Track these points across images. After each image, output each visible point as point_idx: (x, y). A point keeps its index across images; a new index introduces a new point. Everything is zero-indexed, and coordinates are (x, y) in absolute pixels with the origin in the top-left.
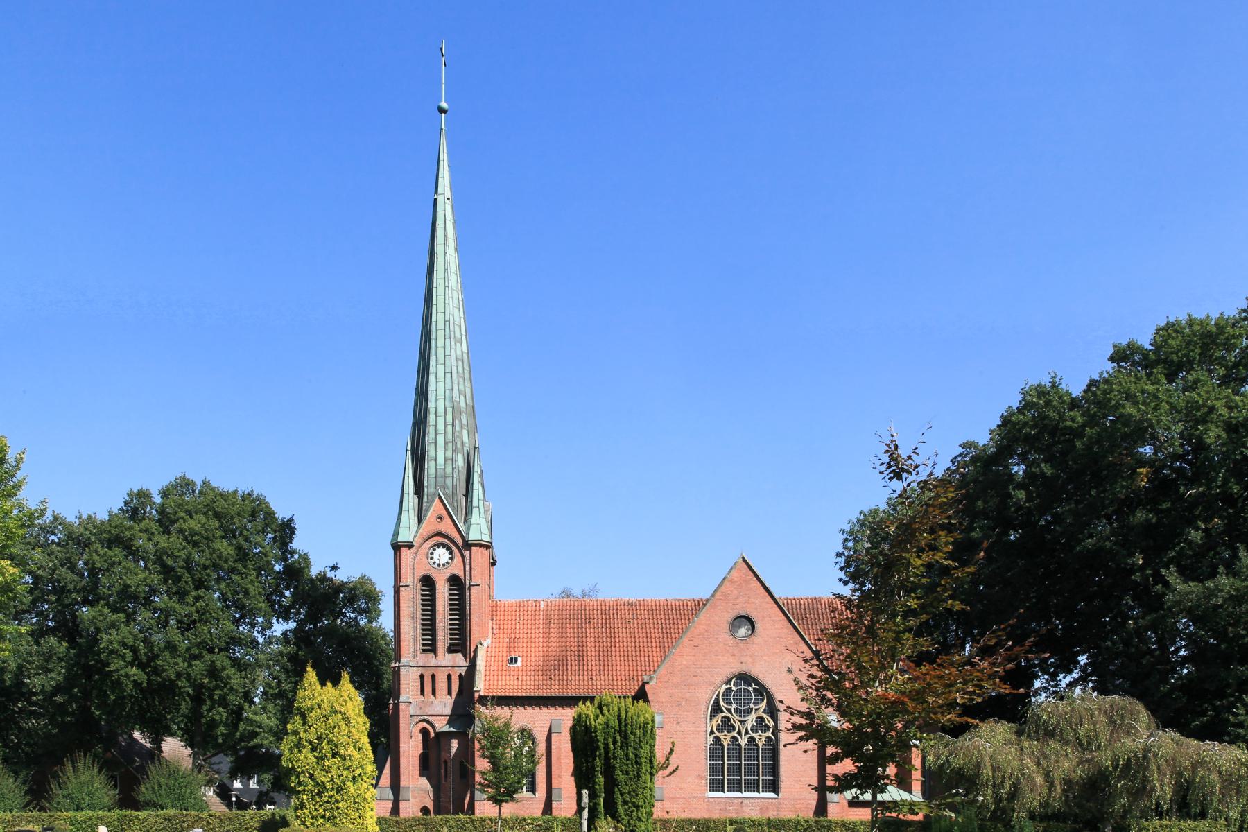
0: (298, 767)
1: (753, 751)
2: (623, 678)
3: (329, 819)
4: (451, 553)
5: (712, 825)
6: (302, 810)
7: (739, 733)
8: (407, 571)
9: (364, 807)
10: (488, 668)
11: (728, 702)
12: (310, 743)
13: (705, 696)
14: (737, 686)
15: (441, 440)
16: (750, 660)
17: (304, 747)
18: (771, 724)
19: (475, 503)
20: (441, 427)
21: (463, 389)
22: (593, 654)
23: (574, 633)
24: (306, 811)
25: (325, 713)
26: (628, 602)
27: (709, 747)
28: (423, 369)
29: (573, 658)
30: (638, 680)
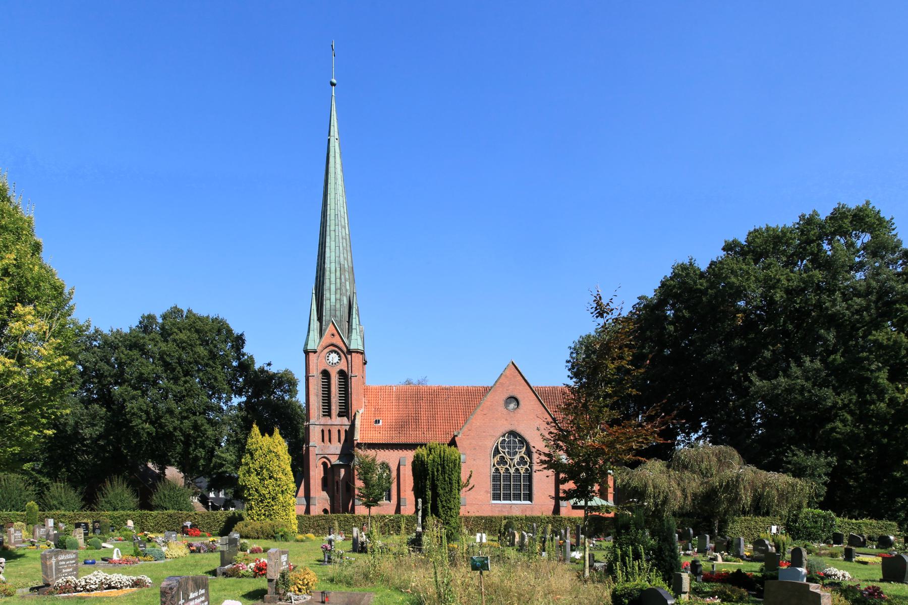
1: (518, 477)
3: (268, 516)
4: (340, 357)
7: (510, 466)
11: (503, 448)
12: (256, 470)
13: (490, 445)
17: (252, 473)
19: (354, 326)
20: (333, 279)
24: (254, 511)
25: (264, 452)
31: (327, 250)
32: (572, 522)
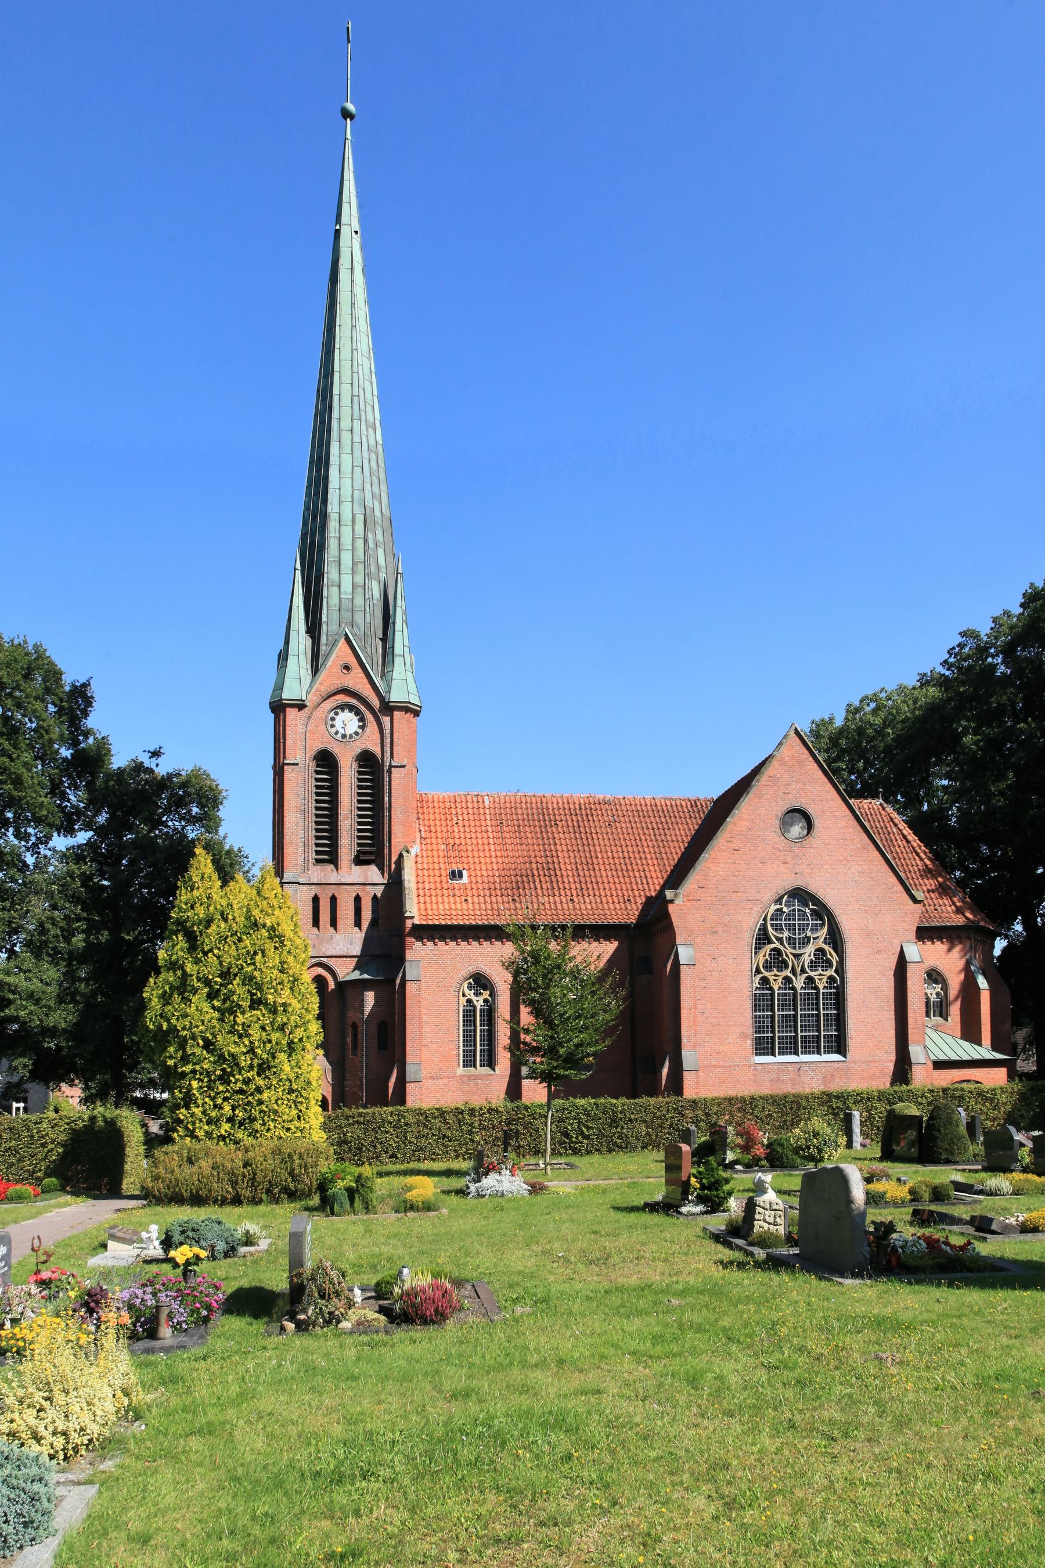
0: (184, 1029)
1: (813, 999)
2: (616, 899)
3: (241, 1124)
4: (362, 719)
6: (188, 1108)
7: (793, 971)
8: (295, 742)
9: (307, 1099)
10: (421, 886)
11: (778, 929)
12: (207, 983)
13: (749, 923)
15: (346, 558)
17: (195, 991)
18: (835, 959)
19: (398, 650)
20: (347, 540)
21: (377, 492)
22: (569, 867)
23: (537, 839)
24: (194, 1110)
25: (235, 927)
26: (604, 800)
28: (319, 459)
29: (541, 873)
30: (636, 903)
31: (333, 472)
32: (987, 1099)
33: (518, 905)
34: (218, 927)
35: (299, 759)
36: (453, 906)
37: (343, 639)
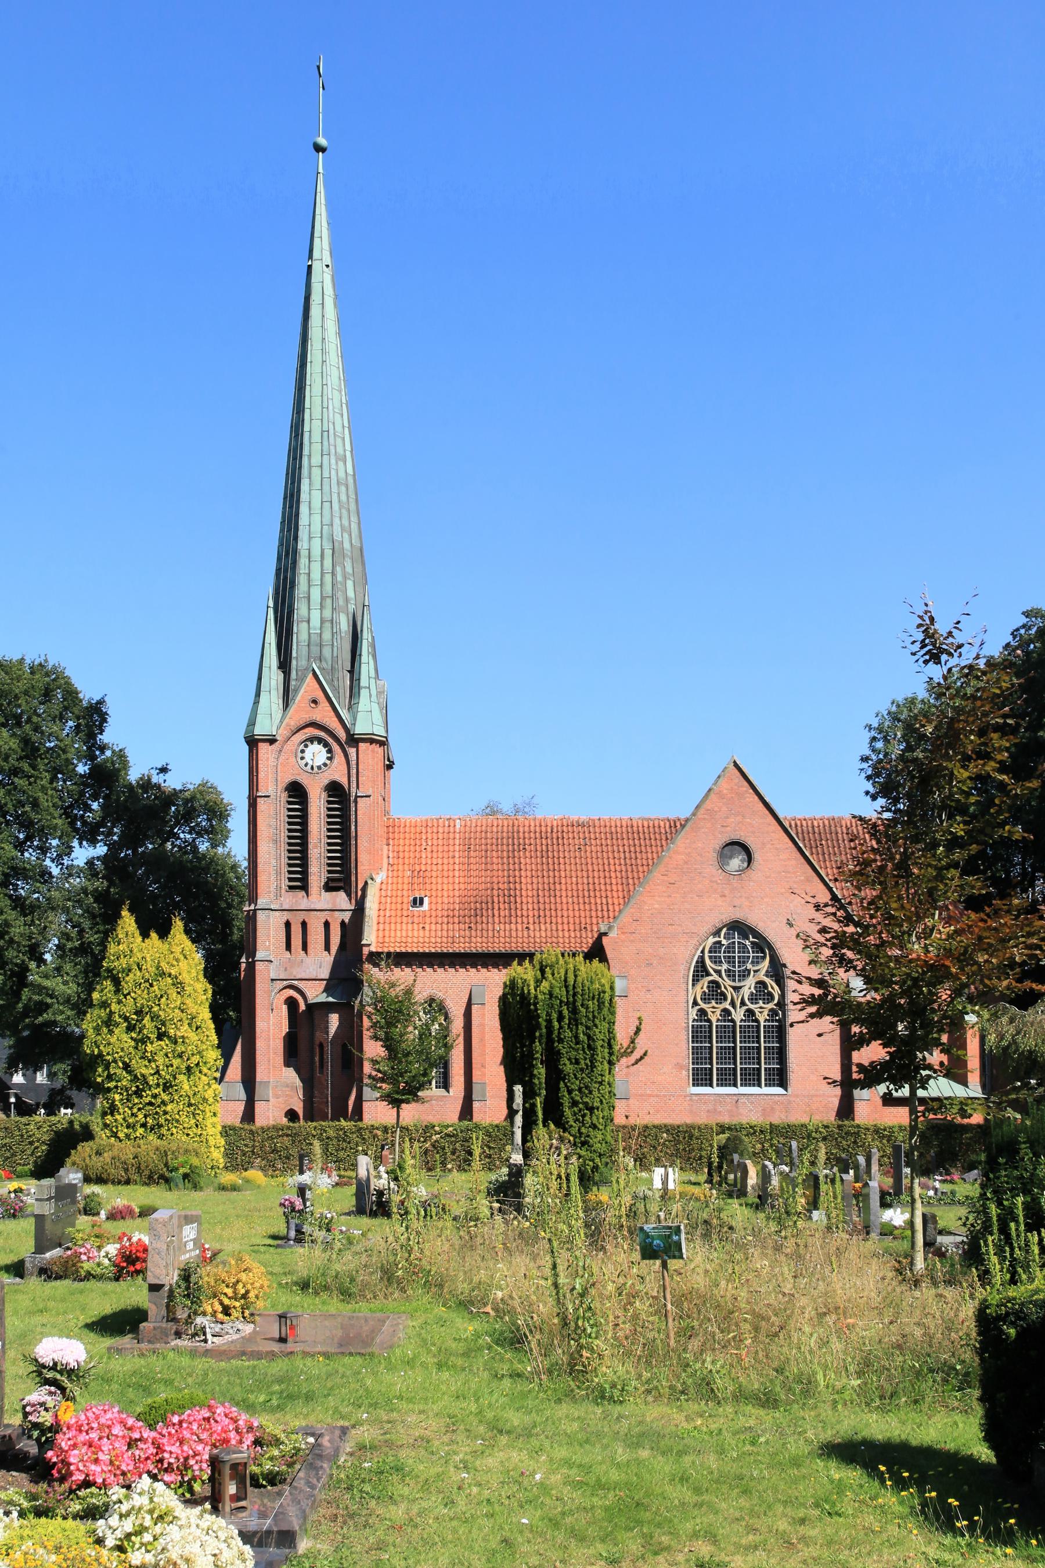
0: (108, 1054)
1: (752, 1031)
3: (152, 1129)
4: (330, 751)
5: (696, 1133)
7: (733, 1004)
8: (267, 775)
11: (716, 961)
12: (126, 1019)
13: (686, 956)
14: (729, 939)
15: (315, 594)
16: (747, 903)
17: (117, 1025)
18: (776, 992)
19: (364, 682)
20: (316, 576)
22: (530, 894)
23: (503, 864)
24: (118, 1117)
25: (147, 976)
26: (578, 822)
27: (691, 1024)
28: (292, 495)
29: (501, 900)
30: (592, 931)
31: (304, 509)
32: (884, 1136)
33: (473, 933)
34: (136, 975)
35: (271, 791)
36: (410, 934)
37: (311, 675)
